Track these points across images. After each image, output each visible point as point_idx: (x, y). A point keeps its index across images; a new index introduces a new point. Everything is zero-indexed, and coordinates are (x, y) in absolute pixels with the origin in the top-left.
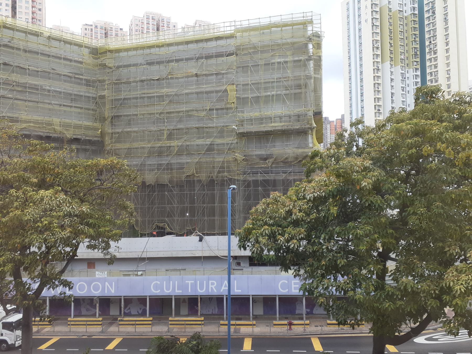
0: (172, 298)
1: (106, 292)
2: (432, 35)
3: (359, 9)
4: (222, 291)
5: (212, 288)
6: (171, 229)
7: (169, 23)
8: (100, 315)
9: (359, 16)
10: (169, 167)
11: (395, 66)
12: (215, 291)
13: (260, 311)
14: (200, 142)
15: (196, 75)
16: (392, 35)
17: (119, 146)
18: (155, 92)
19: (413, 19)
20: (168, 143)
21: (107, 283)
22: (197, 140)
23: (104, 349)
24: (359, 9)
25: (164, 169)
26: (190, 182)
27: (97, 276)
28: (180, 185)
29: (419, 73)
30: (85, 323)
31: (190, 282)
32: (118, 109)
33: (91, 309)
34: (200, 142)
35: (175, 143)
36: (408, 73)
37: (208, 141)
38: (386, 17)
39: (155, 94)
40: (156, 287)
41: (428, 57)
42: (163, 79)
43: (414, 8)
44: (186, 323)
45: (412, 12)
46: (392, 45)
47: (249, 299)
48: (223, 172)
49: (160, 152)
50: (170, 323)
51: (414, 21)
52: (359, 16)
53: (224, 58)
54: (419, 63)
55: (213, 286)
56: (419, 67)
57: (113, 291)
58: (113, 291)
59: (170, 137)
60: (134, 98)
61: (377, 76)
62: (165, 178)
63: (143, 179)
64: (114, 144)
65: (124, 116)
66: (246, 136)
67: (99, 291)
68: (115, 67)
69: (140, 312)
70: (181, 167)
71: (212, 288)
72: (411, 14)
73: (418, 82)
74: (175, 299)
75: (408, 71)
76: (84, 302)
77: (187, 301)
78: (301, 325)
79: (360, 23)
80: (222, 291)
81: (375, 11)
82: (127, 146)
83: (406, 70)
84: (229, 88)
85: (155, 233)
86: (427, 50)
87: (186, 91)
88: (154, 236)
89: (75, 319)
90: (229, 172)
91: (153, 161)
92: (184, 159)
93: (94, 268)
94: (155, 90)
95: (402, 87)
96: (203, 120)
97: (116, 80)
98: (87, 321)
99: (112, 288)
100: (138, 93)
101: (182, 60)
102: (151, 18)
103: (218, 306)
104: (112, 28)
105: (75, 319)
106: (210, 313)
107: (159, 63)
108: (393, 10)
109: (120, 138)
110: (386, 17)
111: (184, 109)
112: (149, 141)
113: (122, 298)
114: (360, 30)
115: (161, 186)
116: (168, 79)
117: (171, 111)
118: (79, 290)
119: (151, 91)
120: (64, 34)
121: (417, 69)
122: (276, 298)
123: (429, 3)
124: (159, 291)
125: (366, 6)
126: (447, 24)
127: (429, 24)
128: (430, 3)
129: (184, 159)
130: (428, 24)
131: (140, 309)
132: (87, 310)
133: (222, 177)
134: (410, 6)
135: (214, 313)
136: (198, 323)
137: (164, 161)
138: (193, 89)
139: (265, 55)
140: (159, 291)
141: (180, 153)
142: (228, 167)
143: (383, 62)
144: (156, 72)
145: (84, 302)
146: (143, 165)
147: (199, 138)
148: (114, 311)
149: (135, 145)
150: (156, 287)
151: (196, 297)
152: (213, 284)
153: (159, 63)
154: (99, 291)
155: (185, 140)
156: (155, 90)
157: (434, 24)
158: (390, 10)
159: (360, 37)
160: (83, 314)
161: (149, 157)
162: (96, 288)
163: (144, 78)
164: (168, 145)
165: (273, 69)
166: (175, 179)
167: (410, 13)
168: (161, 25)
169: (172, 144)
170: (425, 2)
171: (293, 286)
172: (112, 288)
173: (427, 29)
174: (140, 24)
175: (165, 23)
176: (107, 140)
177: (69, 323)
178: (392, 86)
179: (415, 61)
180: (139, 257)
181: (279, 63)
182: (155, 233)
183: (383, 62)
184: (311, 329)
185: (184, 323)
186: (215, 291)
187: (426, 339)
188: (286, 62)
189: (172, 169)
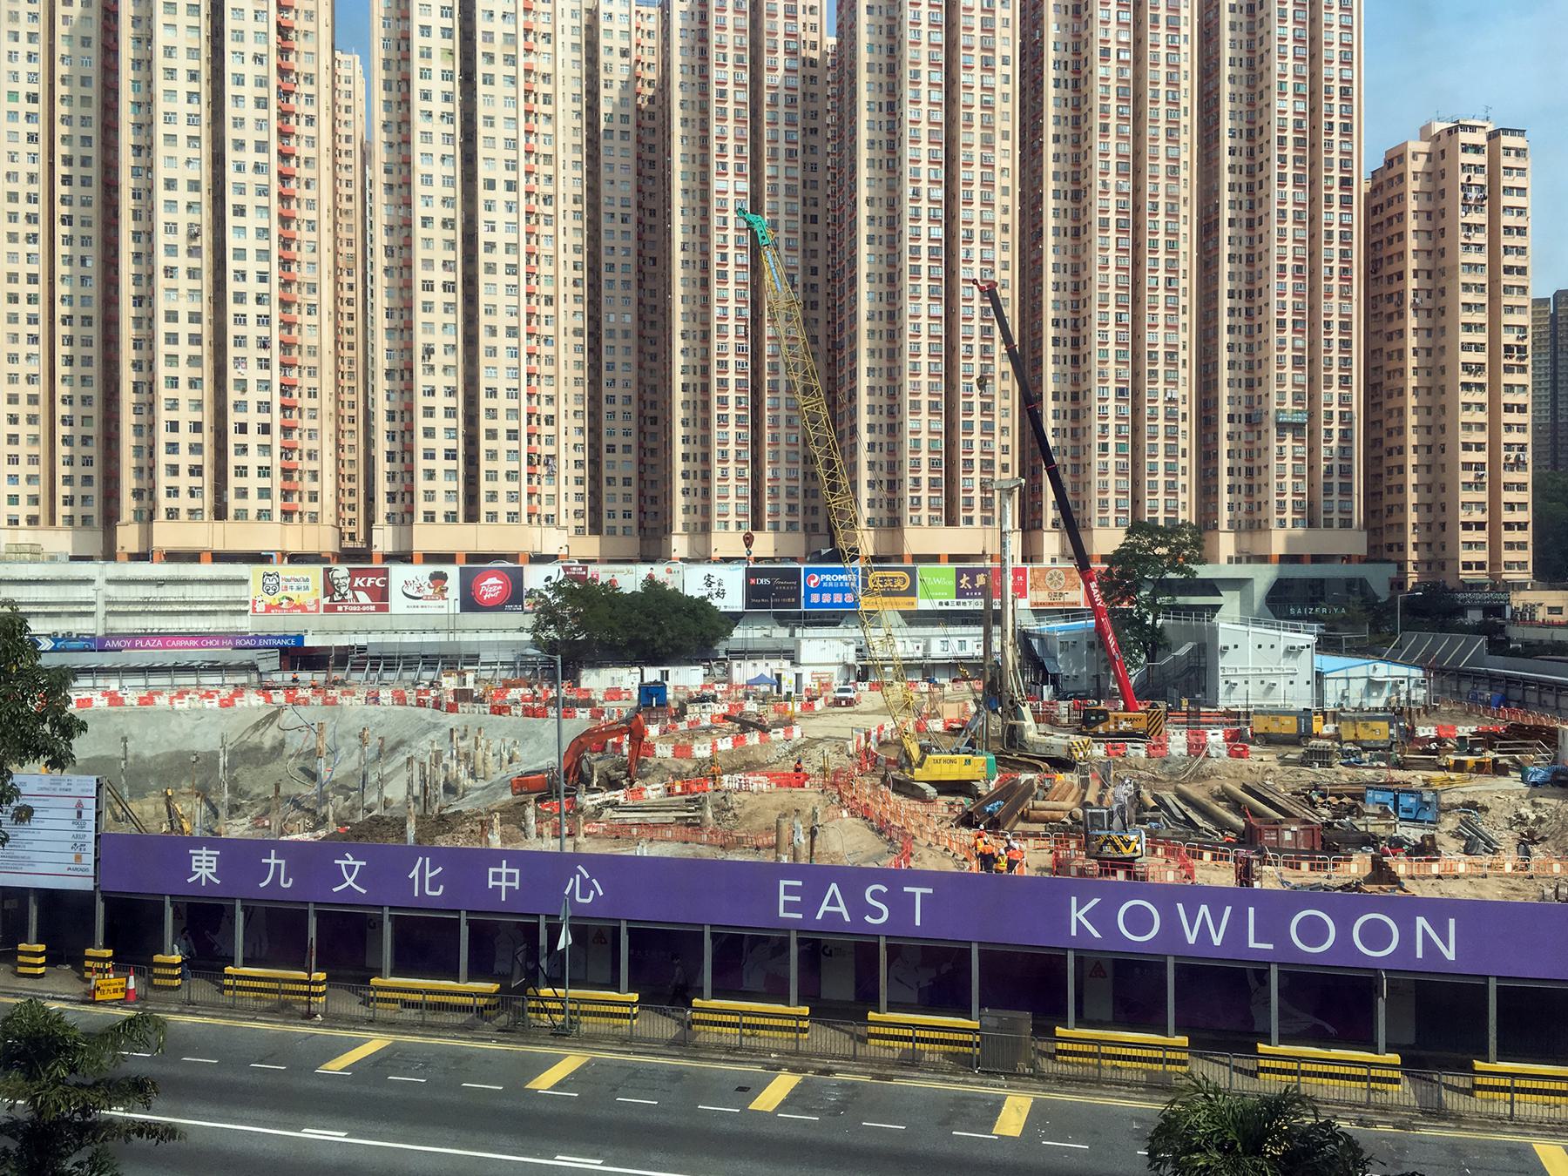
31: (918, 891)
57: (1450, 955)
58: (1450, 955)
113: (1493, 984)
136: (901, 1032)
171: (782, 898)
172: (1446, 945)
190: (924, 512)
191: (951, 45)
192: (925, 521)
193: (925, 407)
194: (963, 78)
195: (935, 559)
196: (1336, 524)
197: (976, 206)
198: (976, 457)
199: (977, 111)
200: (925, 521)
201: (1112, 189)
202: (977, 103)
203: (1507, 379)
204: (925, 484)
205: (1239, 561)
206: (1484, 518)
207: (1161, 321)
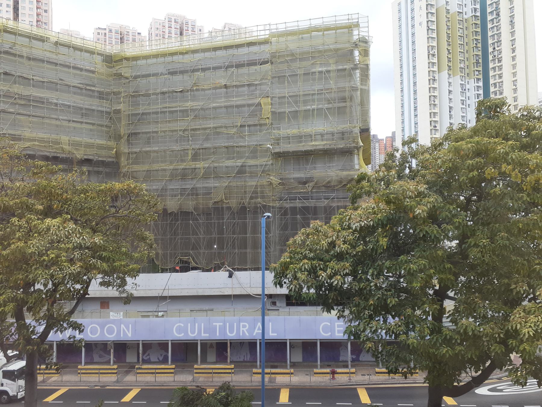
0: (197, 343)
1: (122, 336)
2: (496, 40)
3: (412, 10)
4: (254, 334)
5: (243, 331)
6: (197, 264)
7: (194, 26)
8: (115, 363)
9: (413, 18)
10: (194, 192)
11: (453, 76)
12: (247, 334)
13: (298, 357)
14: (229, 163)
15: (226, 86)
16: (450, 40)
17: (136, 168)
18: (178, 105)
19: (474, 22)
20: (193, 165)
21: (122, 326)
22: (227, 161)
23: (119, 401)
24: (412, 10)
25: (188, 195)
26: (218, 210)
27: (111, 318)
28: (207, 213)
29: (481, 84)
30: (97, 371)
31: (218, 324)
32: (136, 125)
33: (105, 355)
34: (229, 163)
35: (201, 165)
36: (468, 84)
37: (239, 162)
38: (443, 20)
39: (178, 109)
40: (179, 330)
41: (491, 65)
42: (188, 91)
43: (475, 10)
44: (214, 371)
45: (473, 14)
46: (451, 51)
47: (285, 343)
48: (257, 198)
49: (184, 175)
50: (195, 371)
51: (476, 24)
52: (413, 18)
53: (258, 67)
54: (481, 72)
55: (245, 329)
56: (481, 77)
57: (130, 335)
58: (130, 335)
59: (195, 157)
60: (153, 113)
61: (433, 88)
62: (190, 205)
63: (164, 206)
64: (131, 166)
65: (143, 133)
66: (282, 157)
67: (114, 335)
68: (132, 76)
69: (161, 359)
70: (208, 192)
71: (243, 331)
72: (472, 16)
73: (480, 95)
74: (201, 343)
75: (468, 82)
76: (96, 347)
77: (215, 346)
78: (346, 373)
79: (413, 26)
80: (254, 334)
81: (431, 13)
82: (146, 167)
83: (467, 80)
84: (263, 101)
85: (178, 268)
86: (491, 58)
87: (214, 105)
88: (177, 271)
89: (86, 367)
90: (263, 197)
91: (175, 185)
92: (212, 183)
93: (108, 308)
94: (178, 104)
95: (461, 100)
96: (233, 138)
97: (134, 92)
98: (100, 369)
99: (129, 331)
100: (158, 107)
101: (209, 69)
102: (173, 21)
103: (250, 352)
104: (128, 32)
105: (86, 367)
106: (242, 360)
107: (182, 72)
108: (451, 12)
109: (138, 158)
110: (443, 20)
111: (212, 126)
112: (171, 163)
113: (141, 343)
114: (413, 34)
115: (185, 214)
116: (193, 91)
117: (197, 127)
118: (91, 333)
119: (174, 105)
120: (73, 39)
121: (478, 79)
122: (316, 343)
123: (493, 3)
124: (183, 334)
125: (420, 7)
126: (513, 27)
127: (492, 28)
128: (494, 4)
129: (212, 183)
130: (492, 28)
131: (161, 355)
132: (100, 356)
133: (255, 203)
134: (471, 7)
135: (246, 360)
136: (228, 371)
137: (189, 185)
138: (221, 102)
139: (305, 63)
140: (183, 334)
141: (206, 176)
142: (262, 192)
143: (439, 71)
144: (179, 83)
145: (96, 347)
146: (164, 190)
147: (228, 159)
148: (131, 358)
149: (155, 167)
150: (179, 330)
151: (226, 341)
152: (244, 326)
153: (182, 72)
154: (114, 335)
155: (213, 161)
156: (178, 104)
157: (498, 28)
158: (448, 11)
159: (413, 43)
160: (95, 361)
161: (171, 180)
162: (110, 331)
163: (165, 90)
164: (193, 166)
165: (314, 80)
166: (201, 206)
167: (471, 15)
168: (185, 28)
169: (198, 166)
170: (488, 2)
171: (337, 329)
172: (129, 331)
173: (490, 34)
174: (161, 27)
175: (190, 26)
176: (123, 161)
177: (79, 371)
178: (450, 99)
179: (477, 71)
180: (160, 295)
181: (320, 72)
182: (178, 268)
183: (439, 71)
184: (358, 378)
185: (211, 371)
186: (247, 334)
187: (489, 390)
188: (328, 72)
189: (197, 195)
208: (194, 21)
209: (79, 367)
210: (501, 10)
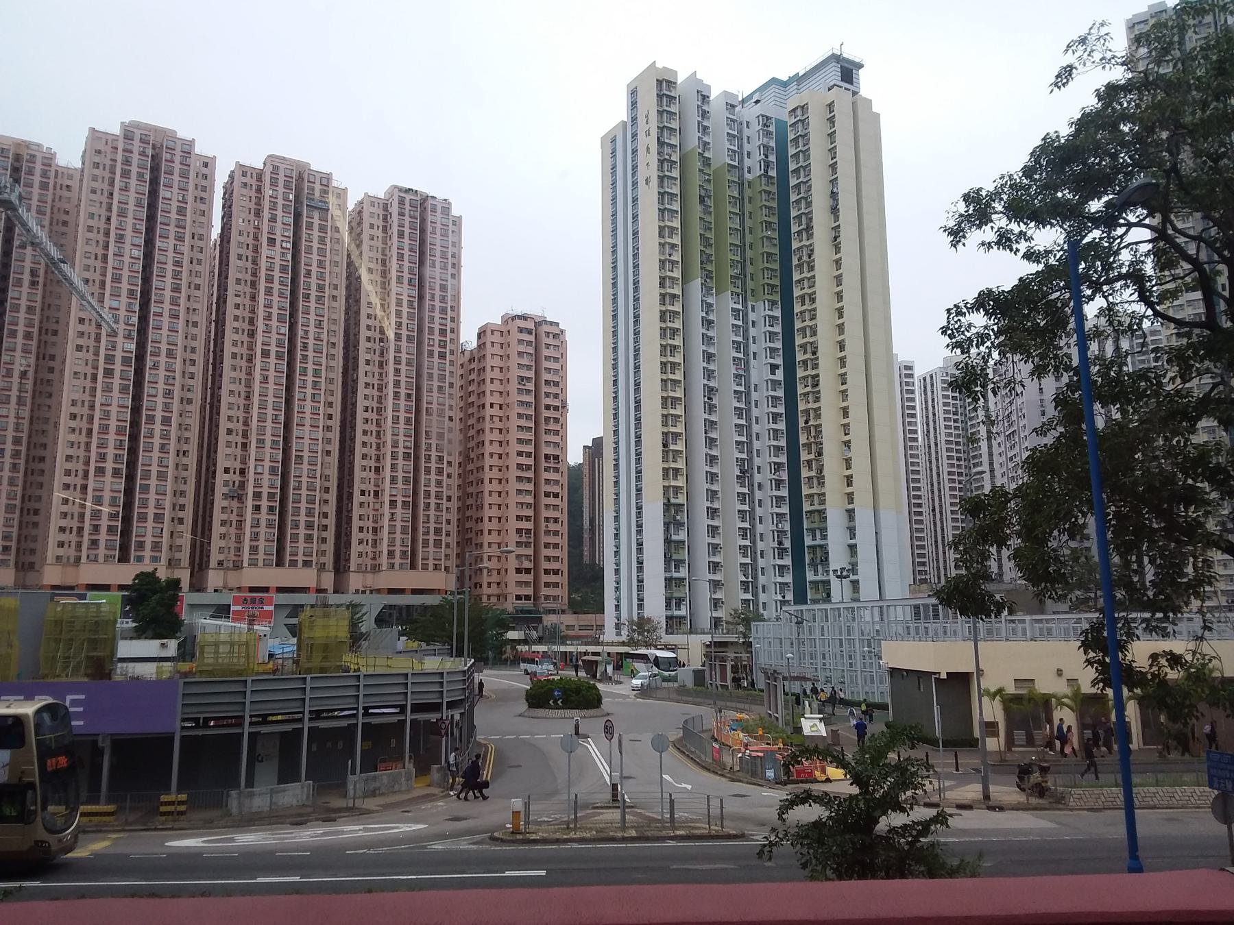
2: (804, 226)
3: (634, 151)
9: (635, 168)
16: (711, 219)
19: (764, 187)
24: (634, 151)
29: (777, 313)
36: (753, 310)
38: (696, 180)
46: (712, 242)
51: (768, 193)
52: (635, 168)
53: (359, 897)
54: (778, 289)
56: (777, 297)
61: (670, 295)
73: (776, 334)
75: (753, 307)
79: (635, 184)
81: (668, 112)
83: (750, 304)
86: (795, 262)
102: (137, 138)
108: (715, 165)
110: (696, 180)
114: (635, 200)
126: (837, 218)
127: (798, 201)
128: (800, 124)
130: (799, 281)
143: (686, 278)
157: (812, 281)
158: (707, 162)
159: (635, 217)
168: (165, 156)
173: (794, 213)
175: (178, 153)
177: (163, 809)
178: (713, 440)
179: (766, 192)
183: (686, 278)
190: (102, 551)
191: (151, 218)
192: (101, 559)
193: (109, 472)
194: (158, 244)
195: (106, 587)
196: (300, 564)
197: (165, 332)
198: (151, 511)
199: (170, 267)
200: (101, 559)
201: (274, 331)
202: (170, 262)
203: (545, 475)
204: (104, 530)
205: (364, 592)
206: (531, 565)
207: (308, 422)
208: (191, 143)
209: (164, 798)
210: (825, 441)
